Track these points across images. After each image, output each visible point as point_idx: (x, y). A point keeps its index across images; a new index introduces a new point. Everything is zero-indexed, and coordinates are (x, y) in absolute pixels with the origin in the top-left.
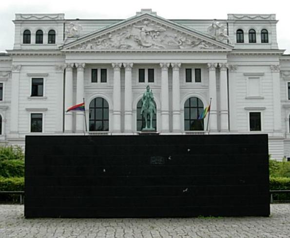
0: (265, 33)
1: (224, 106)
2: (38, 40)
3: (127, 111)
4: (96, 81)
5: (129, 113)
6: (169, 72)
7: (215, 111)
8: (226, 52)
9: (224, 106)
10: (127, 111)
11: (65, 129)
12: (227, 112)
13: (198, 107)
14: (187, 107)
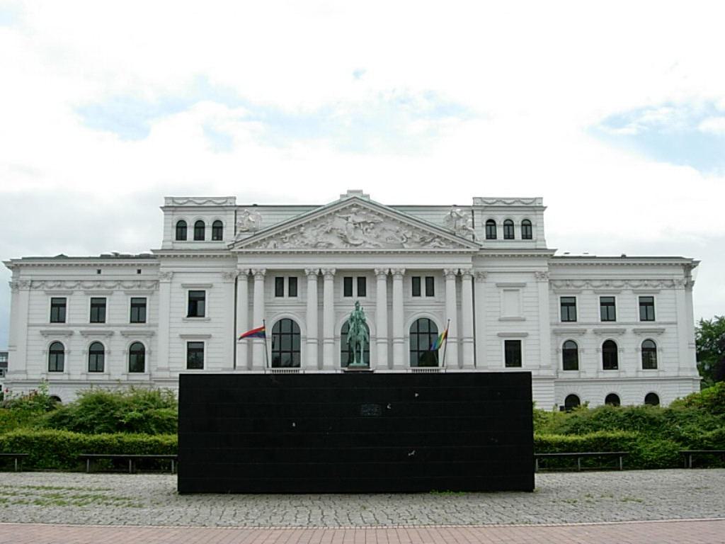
1: (468, 331)
9: (468, 331)
10: (455, 342)
11: (237, 364)
12: (472, 340)
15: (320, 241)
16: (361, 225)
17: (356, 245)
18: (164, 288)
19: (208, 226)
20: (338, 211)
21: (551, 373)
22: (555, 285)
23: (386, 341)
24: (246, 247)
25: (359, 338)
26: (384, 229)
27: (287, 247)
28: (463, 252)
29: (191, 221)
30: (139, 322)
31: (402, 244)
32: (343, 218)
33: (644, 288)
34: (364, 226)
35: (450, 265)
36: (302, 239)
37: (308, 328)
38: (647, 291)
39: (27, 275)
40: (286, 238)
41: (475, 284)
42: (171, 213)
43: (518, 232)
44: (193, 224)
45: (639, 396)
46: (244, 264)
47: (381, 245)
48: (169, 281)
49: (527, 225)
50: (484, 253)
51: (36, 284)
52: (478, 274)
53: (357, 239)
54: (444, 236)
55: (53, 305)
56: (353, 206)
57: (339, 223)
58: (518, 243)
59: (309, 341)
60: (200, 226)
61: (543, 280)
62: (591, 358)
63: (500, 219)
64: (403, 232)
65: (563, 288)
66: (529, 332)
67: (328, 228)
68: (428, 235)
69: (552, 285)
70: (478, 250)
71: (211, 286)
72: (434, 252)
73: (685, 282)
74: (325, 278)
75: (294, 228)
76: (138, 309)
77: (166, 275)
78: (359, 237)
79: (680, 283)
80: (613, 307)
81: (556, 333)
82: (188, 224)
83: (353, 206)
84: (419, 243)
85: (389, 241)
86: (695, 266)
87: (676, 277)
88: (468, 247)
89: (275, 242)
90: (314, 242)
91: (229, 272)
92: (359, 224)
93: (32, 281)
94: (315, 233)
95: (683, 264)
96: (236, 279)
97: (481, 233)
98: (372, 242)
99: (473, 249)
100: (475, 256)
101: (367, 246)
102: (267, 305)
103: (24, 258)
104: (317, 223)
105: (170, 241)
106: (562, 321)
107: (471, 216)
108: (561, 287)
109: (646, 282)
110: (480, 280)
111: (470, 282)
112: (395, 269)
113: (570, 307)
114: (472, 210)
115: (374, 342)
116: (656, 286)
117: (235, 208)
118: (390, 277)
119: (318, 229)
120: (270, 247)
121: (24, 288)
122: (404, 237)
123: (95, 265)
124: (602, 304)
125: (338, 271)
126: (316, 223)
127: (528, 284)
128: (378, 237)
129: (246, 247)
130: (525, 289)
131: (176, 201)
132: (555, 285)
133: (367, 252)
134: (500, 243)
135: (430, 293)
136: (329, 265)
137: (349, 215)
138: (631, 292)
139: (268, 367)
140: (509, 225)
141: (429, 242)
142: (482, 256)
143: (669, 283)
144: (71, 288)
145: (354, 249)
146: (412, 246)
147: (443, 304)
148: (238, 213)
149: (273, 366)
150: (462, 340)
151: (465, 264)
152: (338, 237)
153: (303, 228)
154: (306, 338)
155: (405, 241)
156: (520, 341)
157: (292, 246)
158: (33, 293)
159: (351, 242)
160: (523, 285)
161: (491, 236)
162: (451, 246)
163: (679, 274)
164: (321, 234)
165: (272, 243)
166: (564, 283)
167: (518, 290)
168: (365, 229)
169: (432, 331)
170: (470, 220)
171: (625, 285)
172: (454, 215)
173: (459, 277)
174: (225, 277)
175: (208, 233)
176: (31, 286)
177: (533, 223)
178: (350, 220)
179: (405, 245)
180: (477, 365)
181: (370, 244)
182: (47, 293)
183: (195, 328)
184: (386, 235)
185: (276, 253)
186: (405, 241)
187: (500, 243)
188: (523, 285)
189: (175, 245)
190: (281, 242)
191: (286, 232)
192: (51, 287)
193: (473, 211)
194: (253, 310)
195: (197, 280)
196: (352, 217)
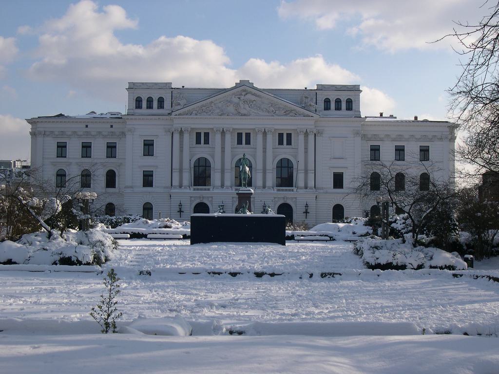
0: (349, 103)
1: (311, 166)
2: (137, 106)
3: (268, 170)
4: (282, 144)
5: (175, 170)
6: (222, 135)
7: (261, 170)
8: (314, 119)
9: (311, 166)
10: (268, 170)
11: (173, 184)
12: (314, 172)
13: (281, 167)
14: (279, 167)
23: (230, 171)
30: (62, 157)
37: (215, 161)
45: (329, 206)
59: (216, 171)
62: (99, 180)
76: (111, 149)
111: (313, 136)
123: (84, 122)
169: (290, 166)
176: (44, 134)
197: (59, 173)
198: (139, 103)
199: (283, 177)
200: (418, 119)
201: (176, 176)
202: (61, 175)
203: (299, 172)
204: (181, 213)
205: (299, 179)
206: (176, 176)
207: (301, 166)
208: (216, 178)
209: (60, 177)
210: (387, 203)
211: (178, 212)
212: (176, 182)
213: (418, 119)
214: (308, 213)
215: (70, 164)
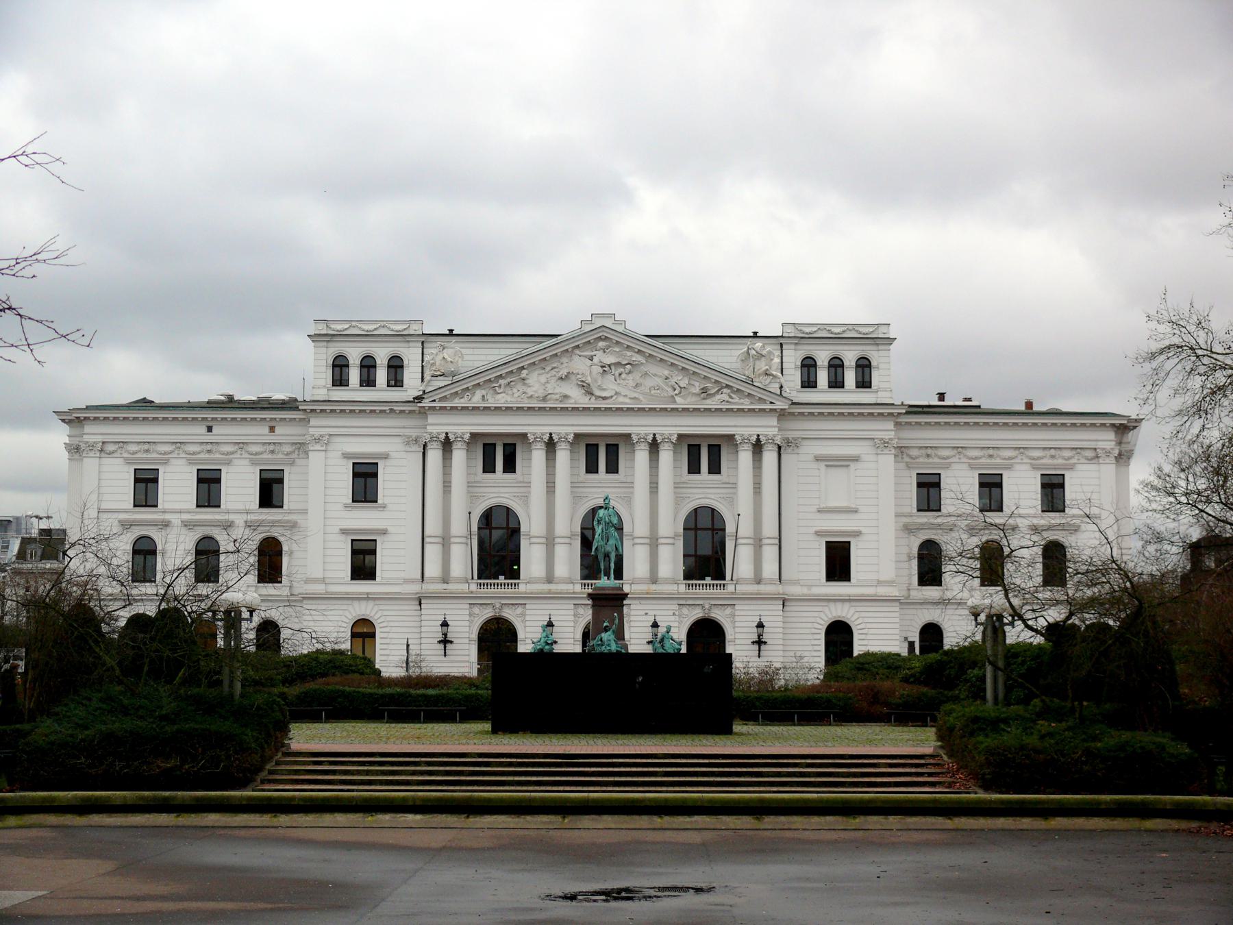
9: (770, 529)
11: (427, 574)
15: (550, 392)
16: (613, 367)
17: (604, 398)
18: (316, 458)
19: (382, 366)
20: (578, 347)
21: (894, 592)
22: (908, 455)
23: (647, 541)
24: (441, 400)
25: (608, 548)
26: (646, 374)
27: (502, 399)
28: (764, 410)
29: (354, 355)
31: (672, 396)
32: (586, 357)
33: (1050, 461)
34: (616, 370)
35: (745, 428)
36: (524, 388)
38: (1052, 465)
39: (94, 433)
40: (500, 386)
41: (783, 456)
42: (325, 344)
43: (850, 377)
44: (358, 362)
46: (438, 425)
47: (641, 397)
48: (323, 448)
49: (864, 366)
50: (797, 410)
51: (110, 448)
52: (788, 442)
53: (604, 390)
54: (736, 386)
55: (137, 480)
56: (600, 338)
57: (579, 364)
58: (850, 394)
59: (533, 540)
60: (368, 365)
61: (886, 451)
63: (823, 357)
64: (675, 379)
65: (921, 460)
66: (864, 530)
67: (564, 372)
68: (714, 382)
69: (905, 456)
70: (787, 407)
71: (386, 457)
72: (721, 410)
73: (1116, 452)
74: (558, 447)
75: (511, 372)
76: (270, 491)
77: (318, 440)
78: (609, 386)
79: (1108, 453)
80: (999, 489)
81: (909, 529)
82: (351, 362)
83: (600, 338)
84: (699, 395)
85: (653, 392)
86: (1135, 427)
87: (1101, 445)
88: (771, 403)
89: (484, 392)
90: (541, 393)
91: (414, 436)
92: (609, 366)
93: (103, 443)
94: (543, 379)
95: (1113, 425)
96: (425, 446)
97: (793, 377)
98: (628, 393)
99: (780, 405)
100: (782, 415)
101: (621, 399)
102: (470, 485)
103: (88, 408)
104: (546, 363)
105: (324, 387)
106: (919, 510)
107: (778, 353)
108: (917, 458)
109: (1053, 451)
110: (790, 450)
111: (775, 455)
112: (662, 435)
113: (931, 490)
114: (780, 341)
115: (631, 542)
116: (1069, 458)
117: (423, 339)
118: (654, 446)
119: (547, 373)
120: (476, 399)
121: (91, 454)
122: (676, 386)
123: (203, 419)
124: (920, 485)
125: (577, 436)
126: (543, 365)
127: (864, 457)
128: (636, 386)
129: (441, 400)
130: (859, 465)
131: (332, 326)
132: (908, 455)
133: (621, 409)
134: (823, 394)
135: (715, 468)
136: (565, 427)
137: (593, 354)
138: (1029, 465)
139: (473, 578)
140: (836, 365)
141: (713, 395)
142: (793, 414)
143: (1090, 454)
144: (228, 454)
145: (603, 404)
146: (689, 400)
147: (734, 486)
148: (425, 345)
149: (479, 578)
150: (760, 540)
151: (768, 428)
152: (578, 384)
153: (525, 372)
154: (529, 537)
155: (677, 392)
156: (849, 542)
157: (509, 399)
158: (107, 461)
159: (598, 393)
160: (856, 459)
161: (809, 383)
162: (747, 401)
163: (1106, 440)
164: (553, 380)
165: (479, 394)
166: (923, 452)
167: (848, 466)
168: (617, 373)
170: (777, 360)
171: (1020, 457)
172: (753, 352)
173: (758, 447)
174: (408, 443)
175: (381, 375)
176: (102, 451)
177: (874, 363)
178: (596, 360)
179: (678, 399)
180: (783, 577)
181: (626, 396)
182: (128, 462)
183: (364, 519)
184: (649, 382)
185: (485, 408)
186: (677, 392)
187: (823, 394)
188: (856, 459)
189: (331, 393)
190: (491, 391)
191: (500, 376)
192: (134, 453)
193: (781, 345)
194: (450, 492)
195: (365, 447)
196: (600, 357)
197: (139, 547)
198: (369, 372)
199: (698, 553)
200: (1036, 408)
201: (433, 552)
202: (144, 552)
203: (740, 541)
204: (448, 646)
205: (739, 561)
206: (433, 552)
207: (746, 529)
208: (532, 559)
209: (142, 557)
210: (1000, 617)
211: (753, 643)
212: (433, 570)
213: (1034, 409)
214: (765, 643)
215: (166, 525)
